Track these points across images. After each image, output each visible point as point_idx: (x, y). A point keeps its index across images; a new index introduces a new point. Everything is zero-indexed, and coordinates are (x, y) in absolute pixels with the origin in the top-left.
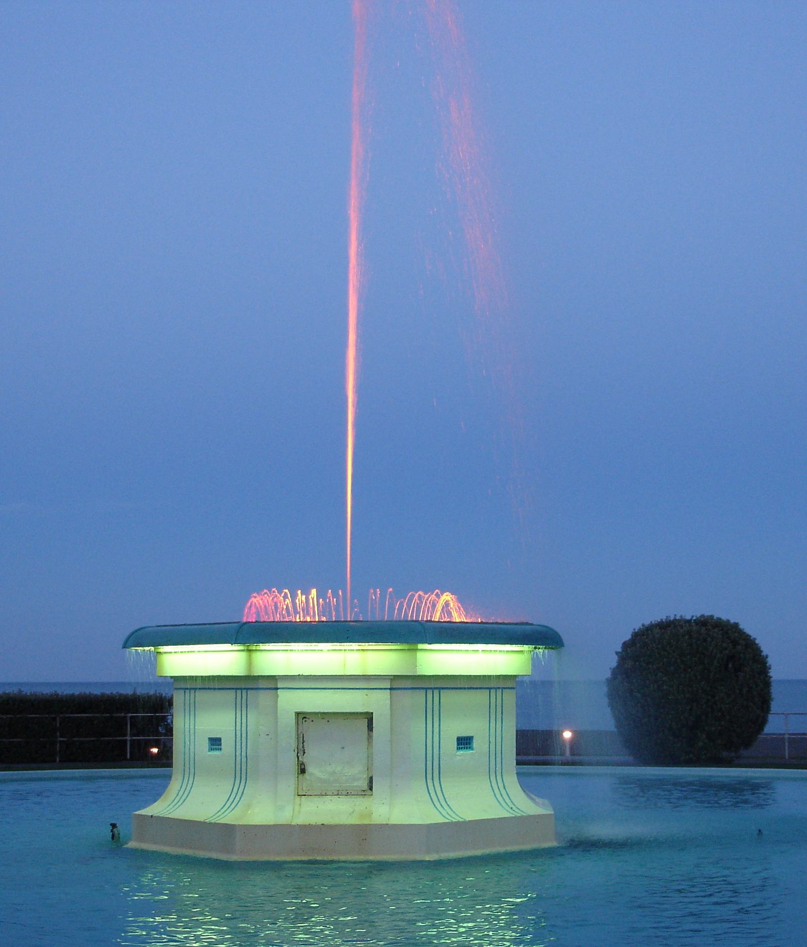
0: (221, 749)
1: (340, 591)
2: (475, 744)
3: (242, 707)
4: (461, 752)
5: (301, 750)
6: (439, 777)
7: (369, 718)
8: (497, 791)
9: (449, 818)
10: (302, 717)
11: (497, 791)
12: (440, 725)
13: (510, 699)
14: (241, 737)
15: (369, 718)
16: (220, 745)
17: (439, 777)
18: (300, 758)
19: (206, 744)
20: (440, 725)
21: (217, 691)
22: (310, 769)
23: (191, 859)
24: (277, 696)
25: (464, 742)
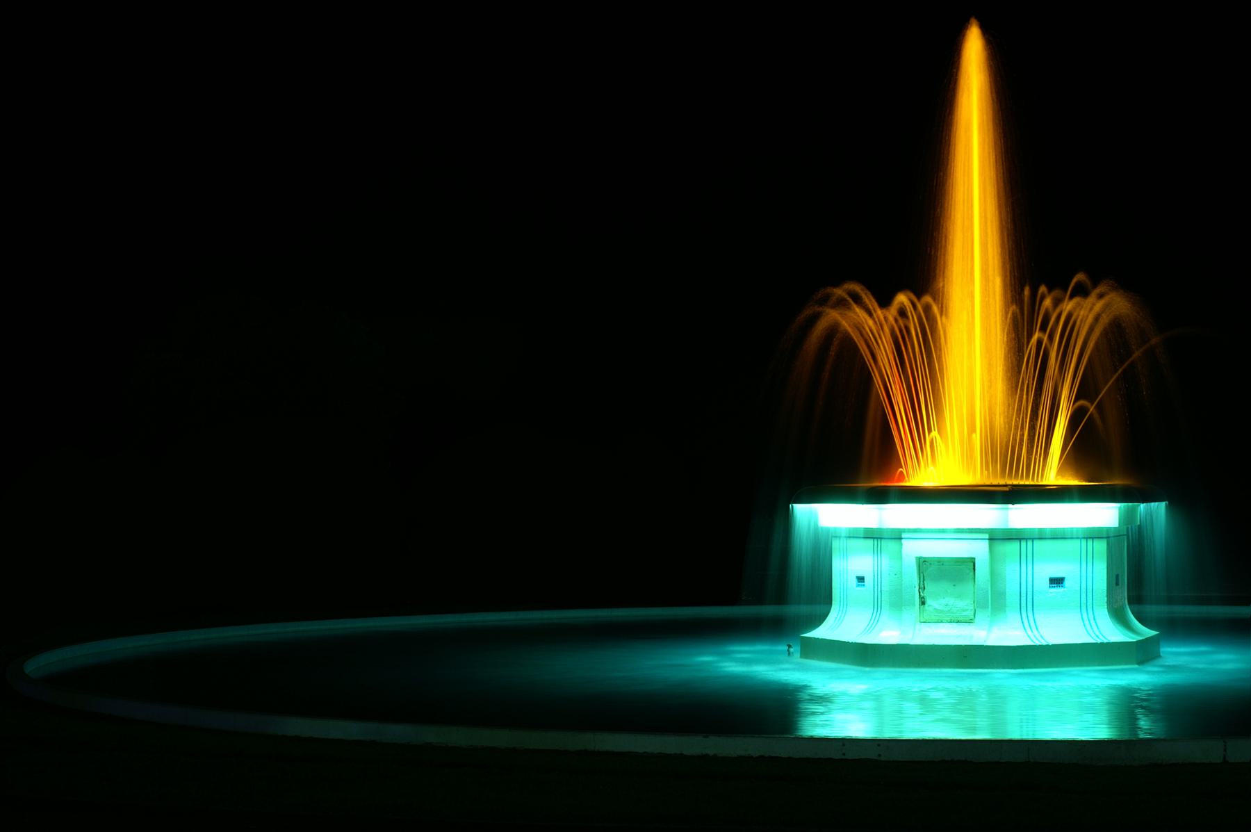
0: (864, 585)
1: (974, 48)
2: (1066, 583)
3: (878, 551)
4: (1053, 590)
5: (922, 588)
6: (1033, 610)
7: (972, 561)
8: (1087, 622)
9: (1035, 640)
10: (922, 563)
11: (1087, 622)
12: (1033, 568)
13: (1101, 547)
14: (878, 576)
15: (972, 561)
16: (864, 582)
17: (1033, 610)
18: (921, 593)
19: (855, 580)
20: (1033, 568)
21: (852, 539)
22: (929, 601)
23: (982, 590)
24: (901, 544)
25: (1057, 582)
